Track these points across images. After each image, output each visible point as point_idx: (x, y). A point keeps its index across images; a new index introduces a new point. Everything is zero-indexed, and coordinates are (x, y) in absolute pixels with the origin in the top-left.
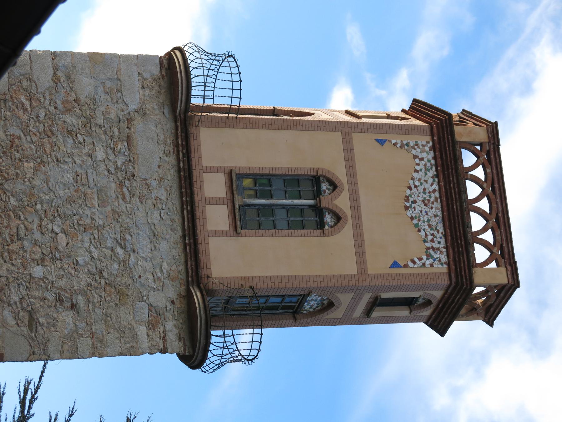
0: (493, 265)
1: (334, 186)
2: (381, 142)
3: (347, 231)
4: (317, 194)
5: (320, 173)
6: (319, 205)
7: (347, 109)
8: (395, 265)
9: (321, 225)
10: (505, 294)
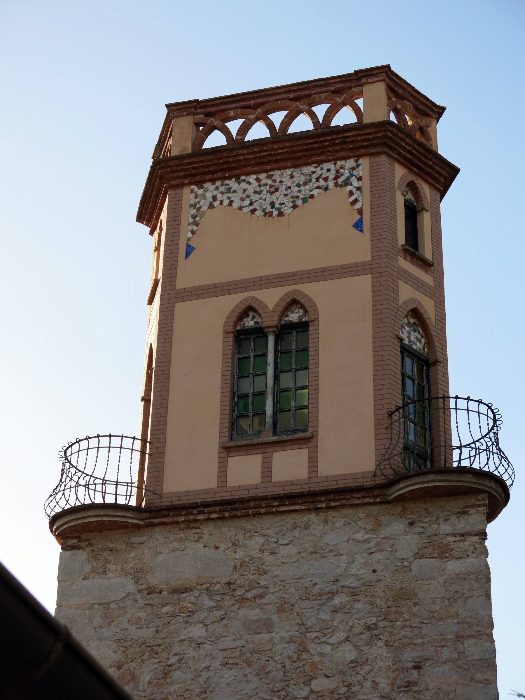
0: (360, 102)
2: (189, 250)
5: (230, 329)
6: (274, 329)
8: (359, 226)
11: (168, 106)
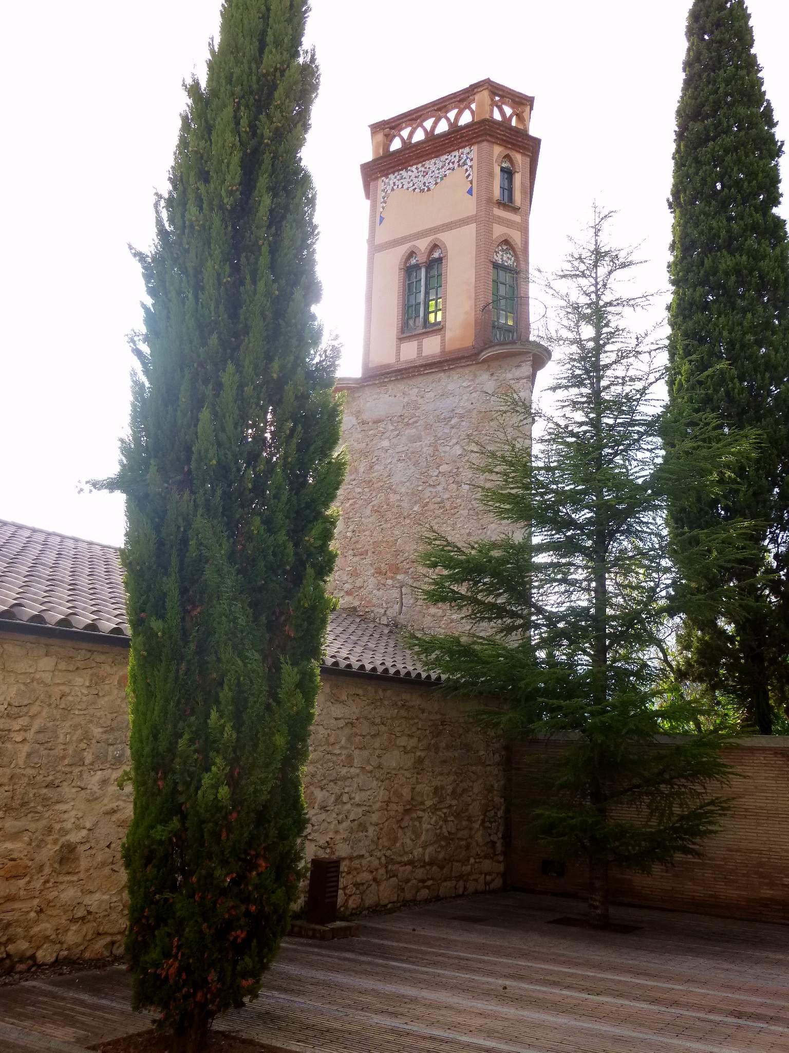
1: (412, 254)
3: (445, 237)
4: (417, 267)
5: (402, 267)
7: (758, 56)
8: (470, 192)
10: (413, 114)
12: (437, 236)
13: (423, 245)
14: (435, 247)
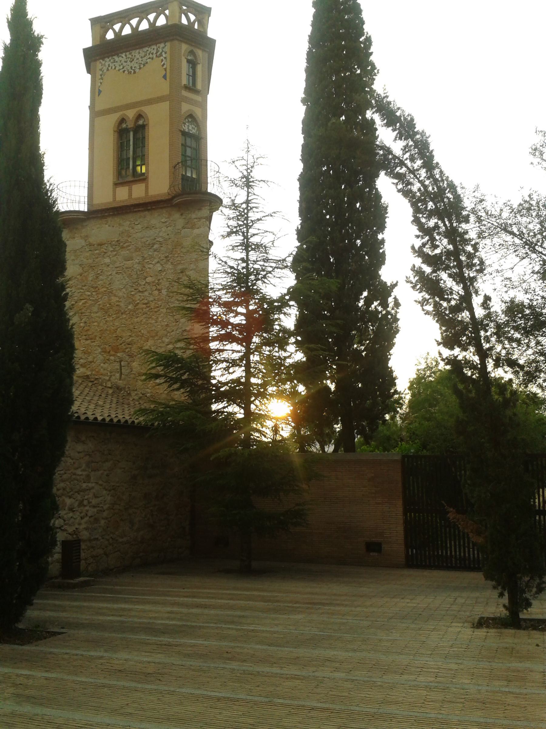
3: (147, 110)
5: (116, 129)
8: (165, 77)
9: (143, 127)
11: (90, 20)
12: (125, 112)
13: (131, 114)
14: (139, 116)
